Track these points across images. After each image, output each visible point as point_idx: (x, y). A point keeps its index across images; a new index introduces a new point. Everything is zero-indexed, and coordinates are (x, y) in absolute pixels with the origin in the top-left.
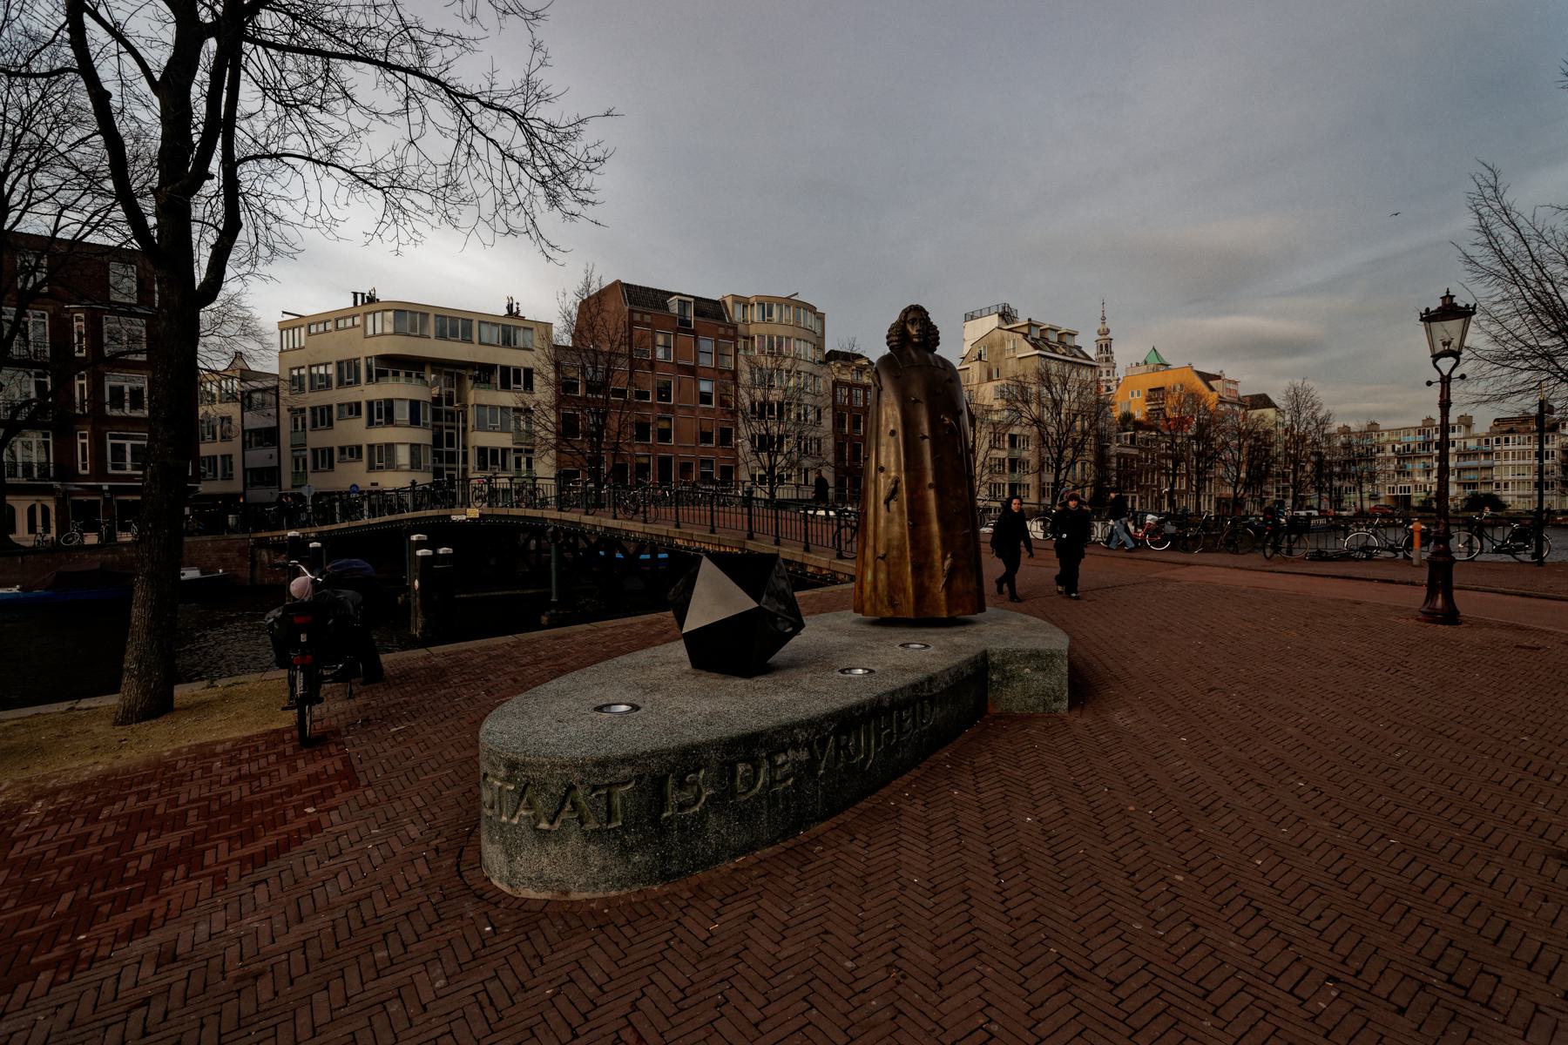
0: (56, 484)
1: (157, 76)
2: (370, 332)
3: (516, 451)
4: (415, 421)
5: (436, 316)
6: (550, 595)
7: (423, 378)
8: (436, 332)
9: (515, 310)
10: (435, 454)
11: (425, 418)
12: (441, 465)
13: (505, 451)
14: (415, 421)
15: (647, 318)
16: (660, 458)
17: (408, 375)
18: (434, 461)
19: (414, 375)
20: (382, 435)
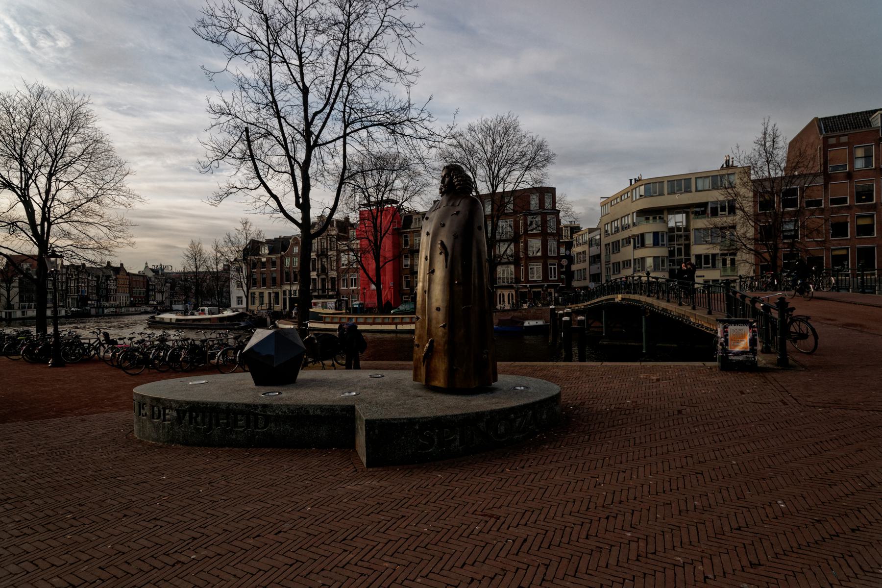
0: (514, 285)
1: (300, 222)
2: (634, 199)
3: (722, 255)
4: (656, 243)
5: (668, 181)
6: (642, 347)
7: (663, 218)
8: (668, 191)
9: (731, 163)
10: (671, 261)
11: (663, 241)
12: (674, 267)
13: (714, 256)
14: (656, 243)
15: (844, 139)
16: (859, 249)
17: (655, 218)
18: (670, 265)
19: (658, 218)
20: (640, 253)
